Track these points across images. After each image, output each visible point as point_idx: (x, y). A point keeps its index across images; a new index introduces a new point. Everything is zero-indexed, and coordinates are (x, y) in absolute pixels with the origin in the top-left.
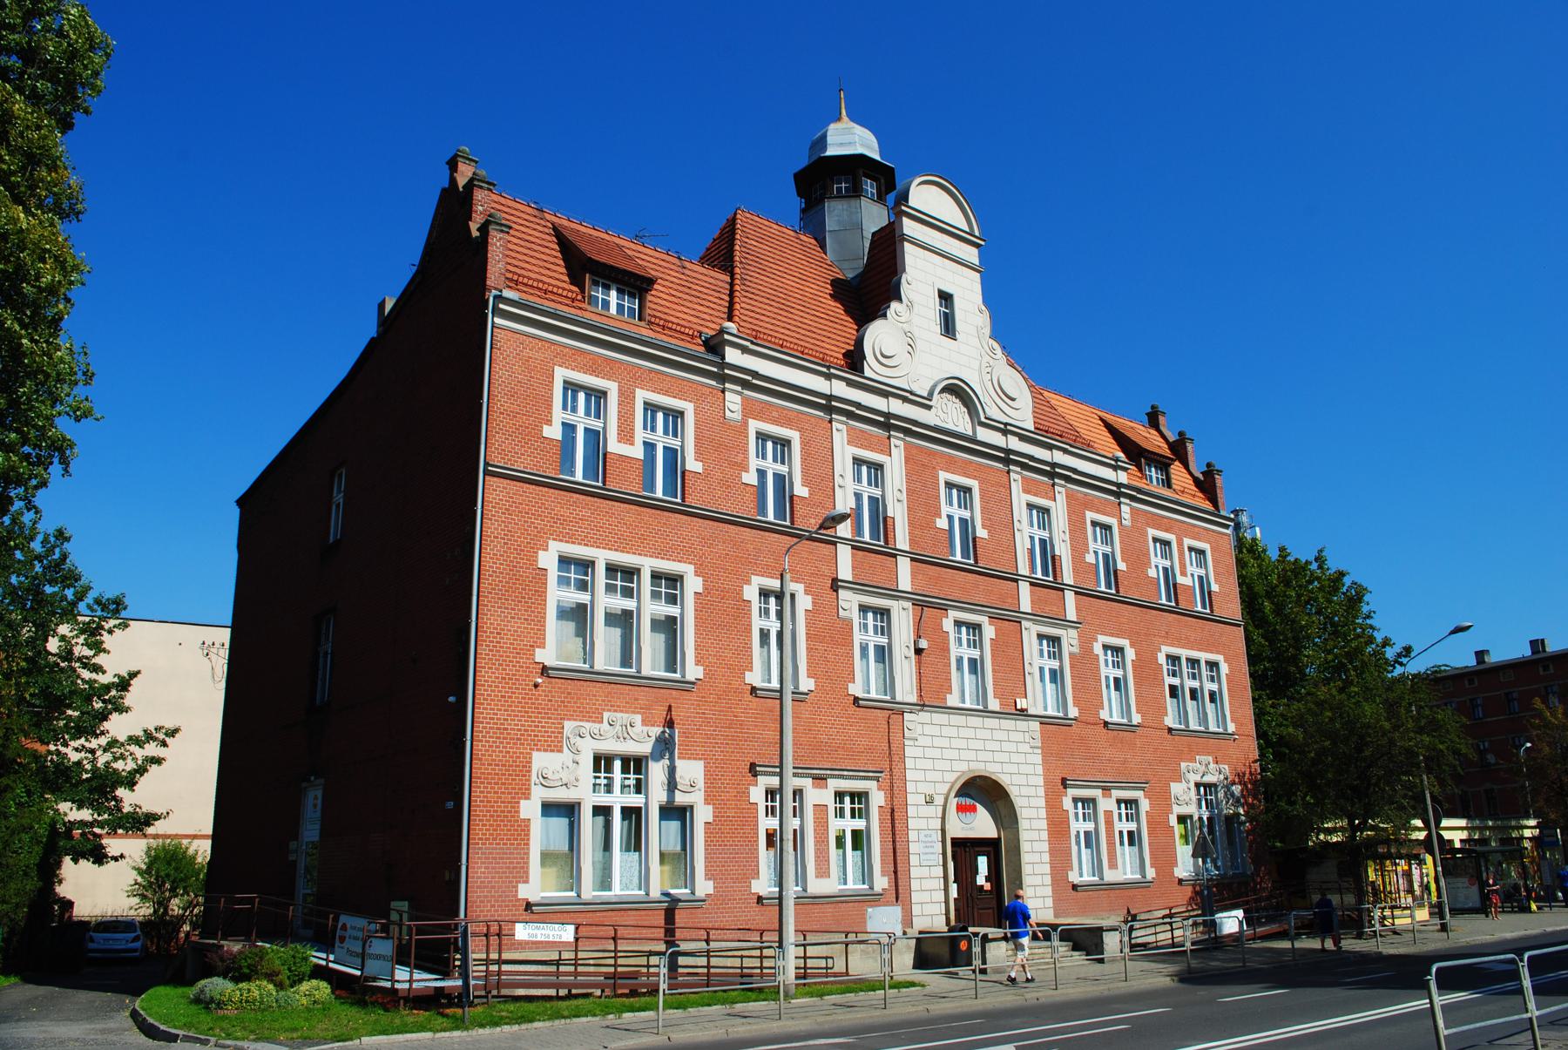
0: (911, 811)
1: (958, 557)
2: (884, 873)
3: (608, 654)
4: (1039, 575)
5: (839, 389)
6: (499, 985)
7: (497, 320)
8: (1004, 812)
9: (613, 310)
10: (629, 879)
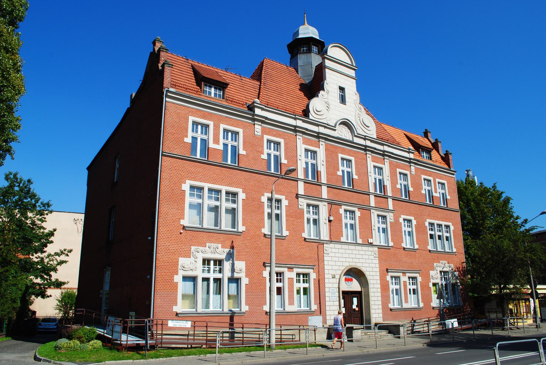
0: (326, 281)
1: (346, 186)
2: (315, 304)
3: (325, 234)
4: (378, 193)
5: (299, 123)
6: (161, 343)
7: (167, 99)
8: (363, 281)
9: (213, 95)
10: (217, 304)
